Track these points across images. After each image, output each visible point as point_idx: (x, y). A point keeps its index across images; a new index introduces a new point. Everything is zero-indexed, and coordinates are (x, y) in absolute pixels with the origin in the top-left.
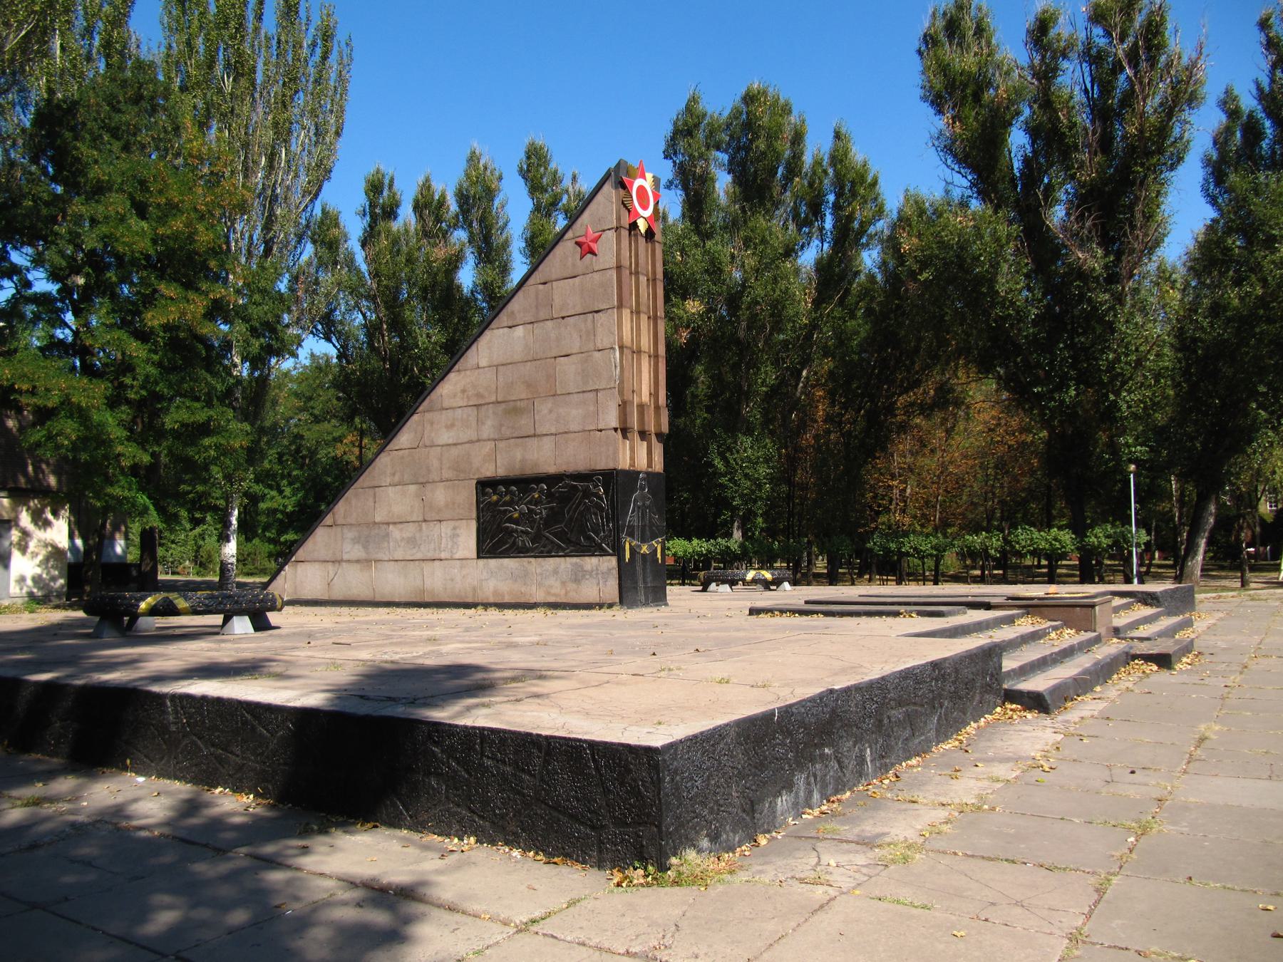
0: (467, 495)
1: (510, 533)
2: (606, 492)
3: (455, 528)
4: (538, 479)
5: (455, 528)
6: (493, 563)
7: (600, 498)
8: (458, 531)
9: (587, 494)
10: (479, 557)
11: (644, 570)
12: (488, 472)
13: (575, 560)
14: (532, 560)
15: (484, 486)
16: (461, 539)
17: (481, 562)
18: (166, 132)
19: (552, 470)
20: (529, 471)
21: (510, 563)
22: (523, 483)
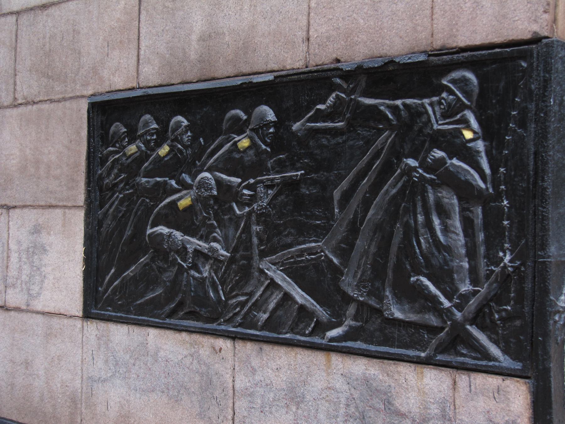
0: (66, 142)
1: (161, 250)
2: (488, 132)
3: (37, 230)
4: (249, 92)
5: (37, 230)
6: (122, 336)
7: (469, 157)
8: (44, 238)
9: (413, 134)
10: (87, 315)
11: (131, 226)
12: (119, 75)
13: (359, 367)
14: (224, 344)
15: (109, 115)
16: (51, 259)
17: (94, 328)
18: (116, 40)
19: (293, 59)
20: (226, 69)
21: (168, 347)
22: (204, 107)
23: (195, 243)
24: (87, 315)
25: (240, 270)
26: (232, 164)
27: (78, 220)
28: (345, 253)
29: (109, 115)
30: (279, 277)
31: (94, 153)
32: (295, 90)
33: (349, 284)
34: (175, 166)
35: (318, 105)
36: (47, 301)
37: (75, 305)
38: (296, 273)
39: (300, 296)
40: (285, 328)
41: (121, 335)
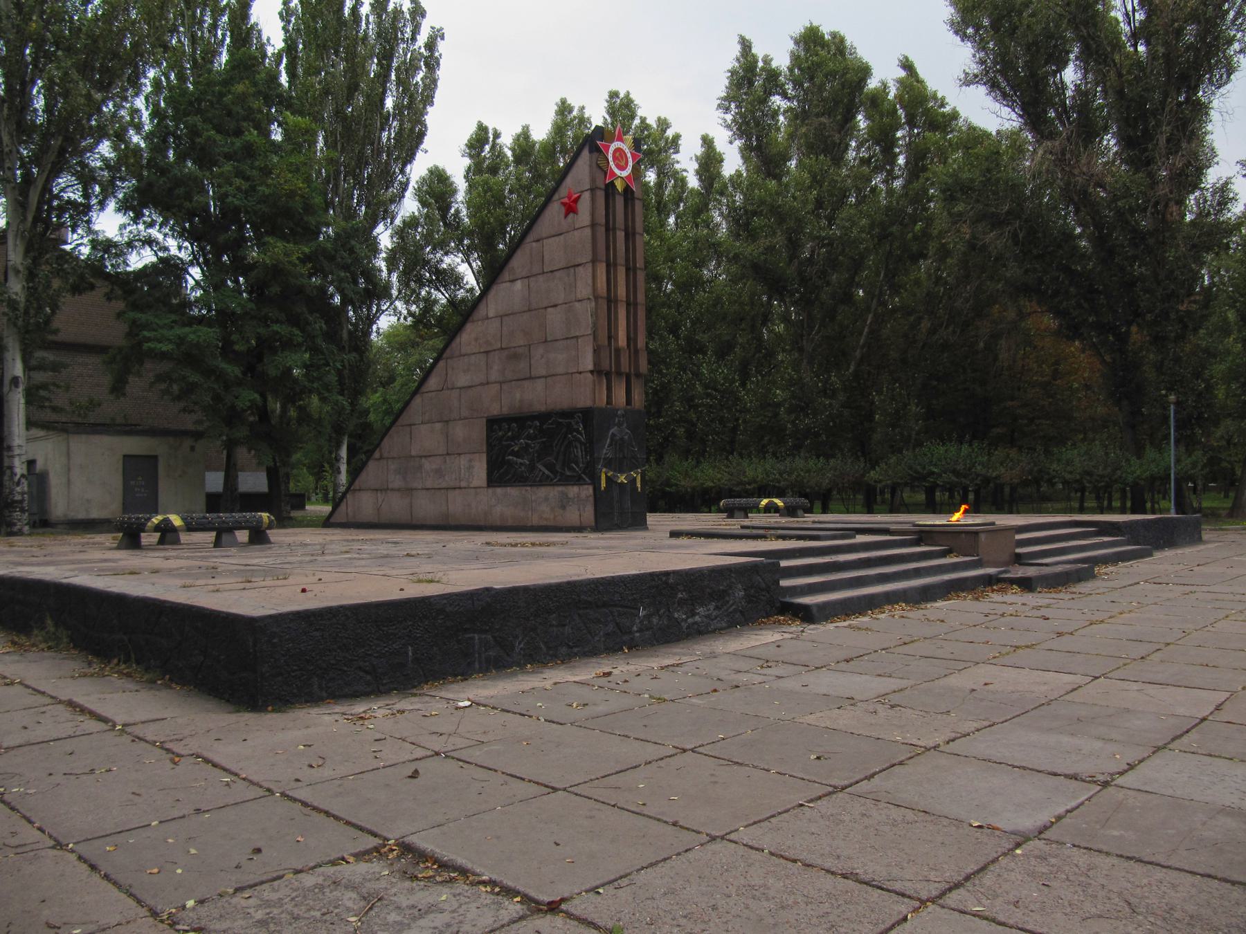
0: (478, 432)
2: (585, 428)
3: (470, 461)
5: (470, 461)
10: (489, 486)
12: (495, 410)
13: (560, 488)
15: (493, 423)
17: (490, 490)
21: (513, 492)
23: (520, 461)
24: (489, 486)
25: (532, 468)
26: (529, 437)
27: (484, 457)
28: (556, 459)
29: (493, 423)
30: (543, 469)
31: (409, 107)
32: (544, 417)
33: (558, 468)
34: (513, 439)
35: (975, 137)
36: (475, 483)
37: (485, 484)
38: (545, 466)
39: (547, 472)
40: (543, 482)
41: (499, 490)
